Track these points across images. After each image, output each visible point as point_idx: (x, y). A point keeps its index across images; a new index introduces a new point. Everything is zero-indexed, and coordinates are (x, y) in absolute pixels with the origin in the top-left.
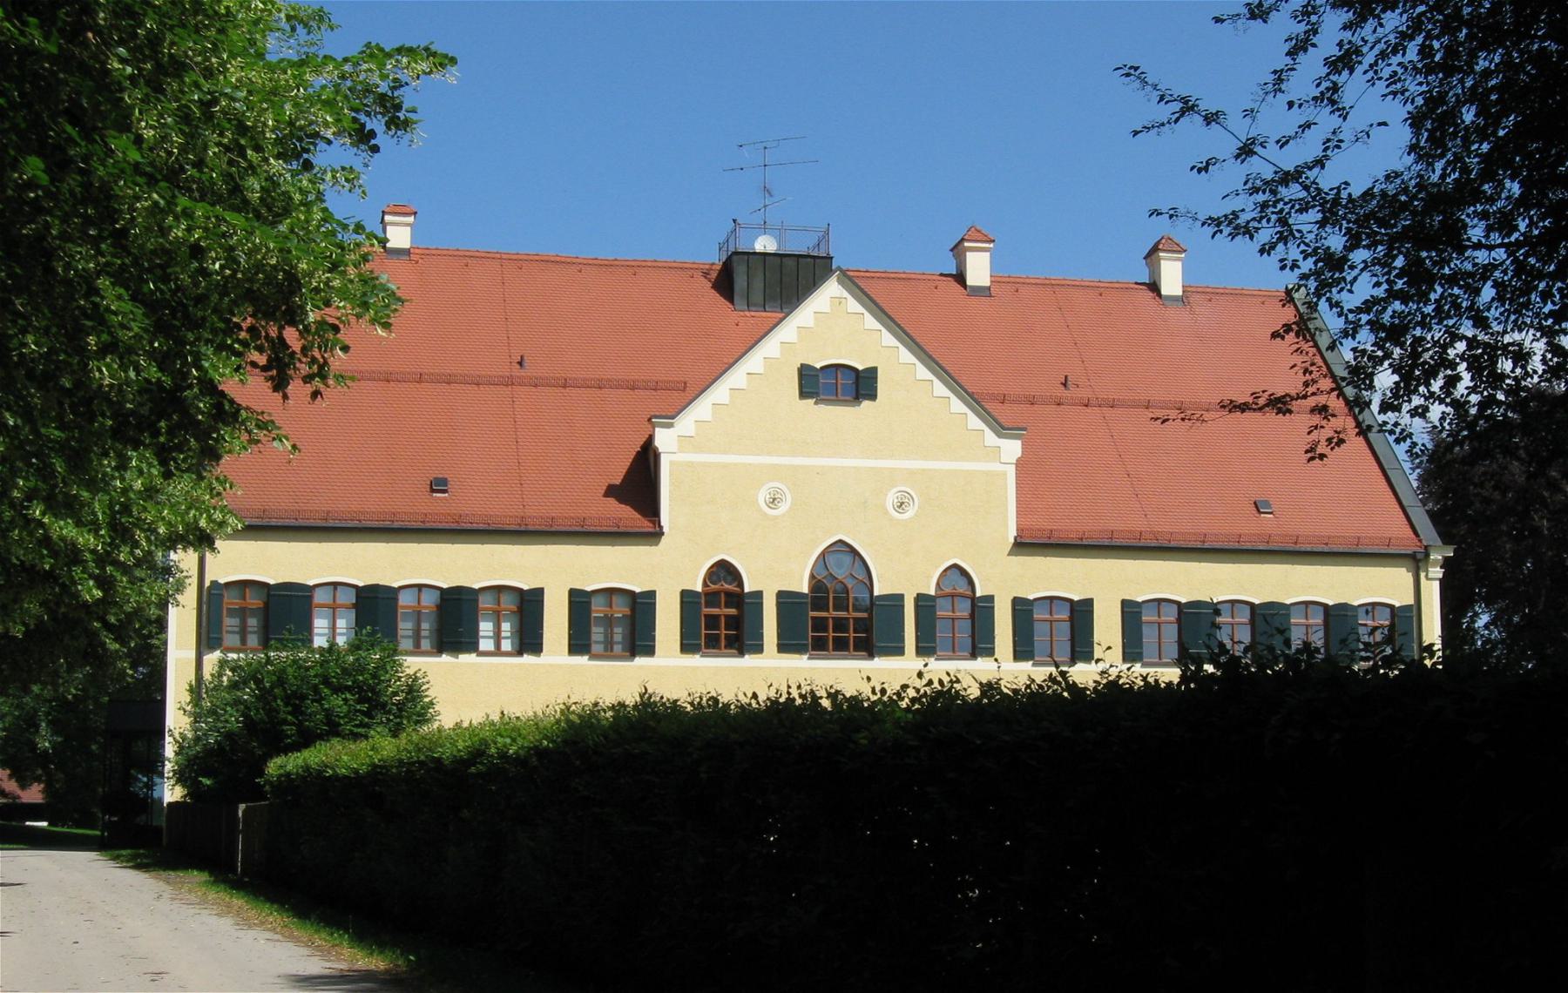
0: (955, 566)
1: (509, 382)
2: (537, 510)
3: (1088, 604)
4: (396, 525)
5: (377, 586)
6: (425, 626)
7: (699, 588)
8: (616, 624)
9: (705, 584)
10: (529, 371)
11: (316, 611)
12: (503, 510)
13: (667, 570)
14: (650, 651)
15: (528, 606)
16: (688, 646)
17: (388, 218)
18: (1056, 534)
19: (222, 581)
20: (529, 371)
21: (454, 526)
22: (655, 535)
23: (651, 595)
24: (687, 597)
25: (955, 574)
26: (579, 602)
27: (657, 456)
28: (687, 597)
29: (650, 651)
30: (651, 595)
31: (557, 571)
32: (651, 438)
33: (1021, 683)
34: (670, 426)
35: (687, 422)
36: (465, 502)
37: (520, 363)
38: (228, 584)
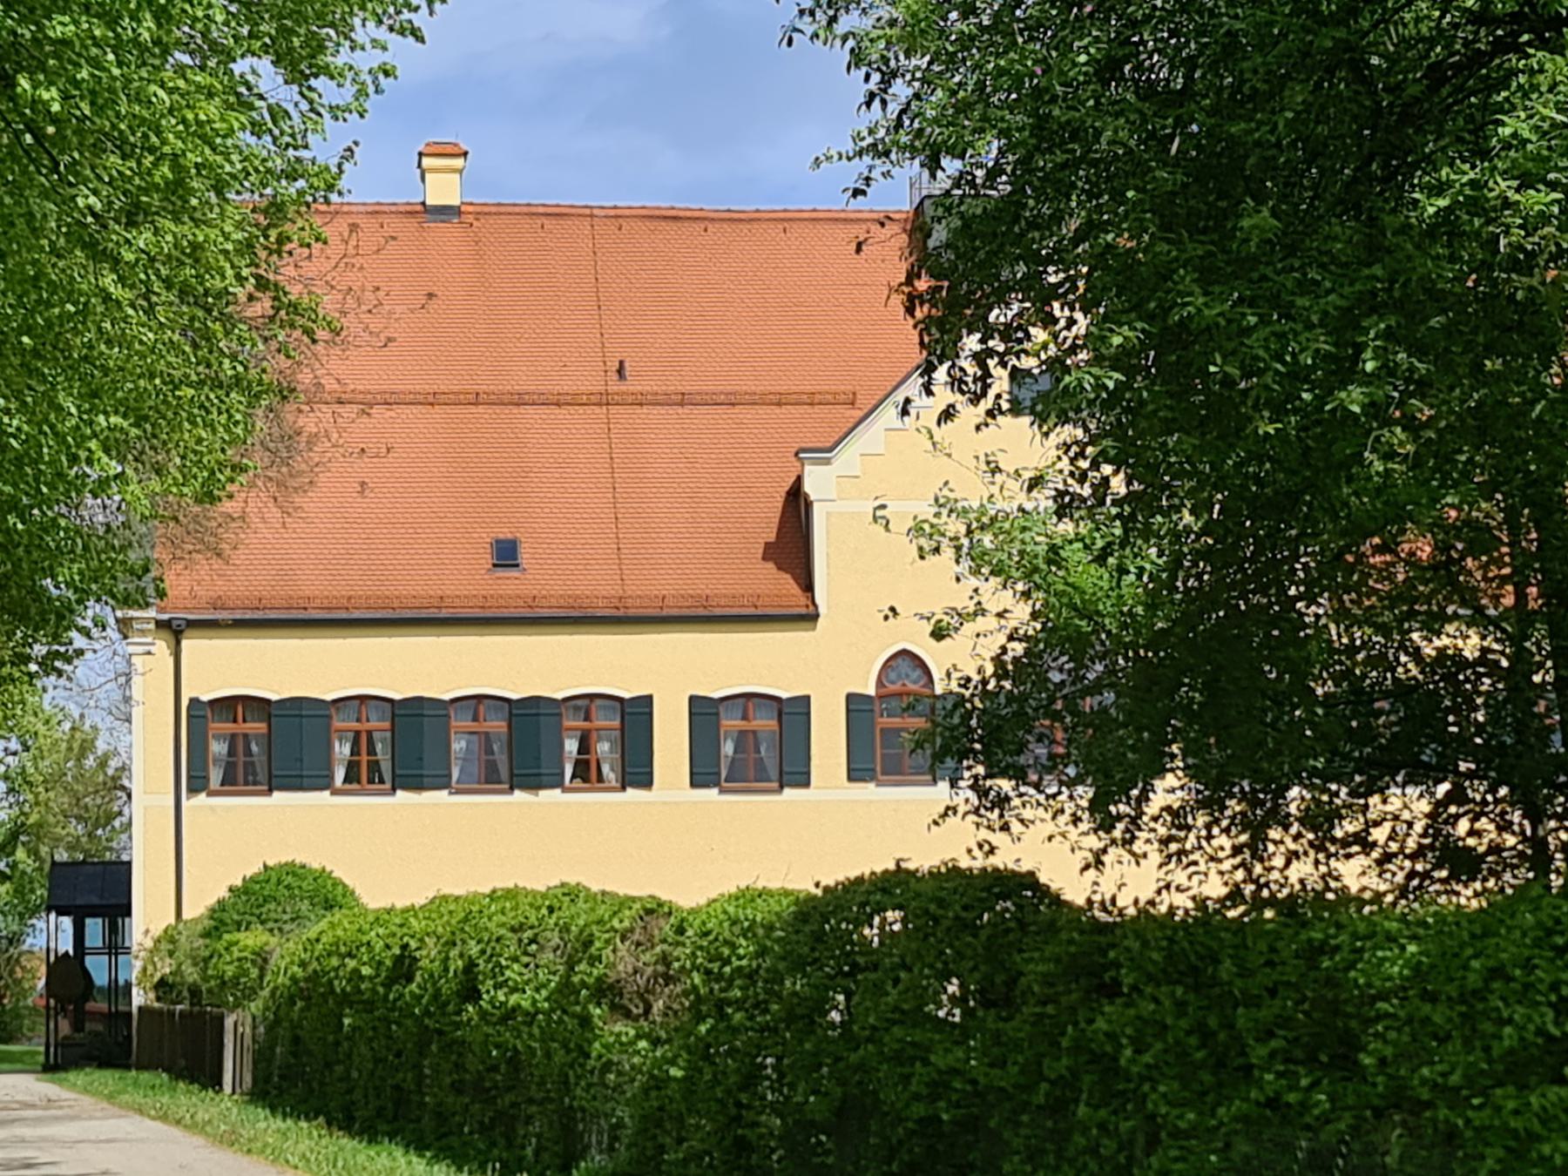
0: (904, 653)
1: (605, 400)
2: (647, 586)
3: (802, 705)
4: (444, 613)
5: (419, 700)
6: (603, 748)
7: (871, 690)
8: (752, 746)
9: (880, 683)
10: (632, 385)
11: (565, 734)
12: (598, 587)
13: (824, 667)
14: (646, 782)
15: (635, 716)
16: (855, 774)
17: (426, 162)
18: (669, 602)
19: (205, 698)
20: (632, 385)
21: (701, 612)
22: (811, 618)
23: (805, 700)
24: (854, 702)
25: (904, 665)
26: (703, 712)
27: (809, 505)
28: (854, 702)
29: (646, 782)
30: (805, 700)
31: (671, 671)
32: (799, 479)
33: (1029, 806)
34: (827, 462)
35: (848, 456)
36: (536, 580)
37: (620, 371)
38: (213, 702)
